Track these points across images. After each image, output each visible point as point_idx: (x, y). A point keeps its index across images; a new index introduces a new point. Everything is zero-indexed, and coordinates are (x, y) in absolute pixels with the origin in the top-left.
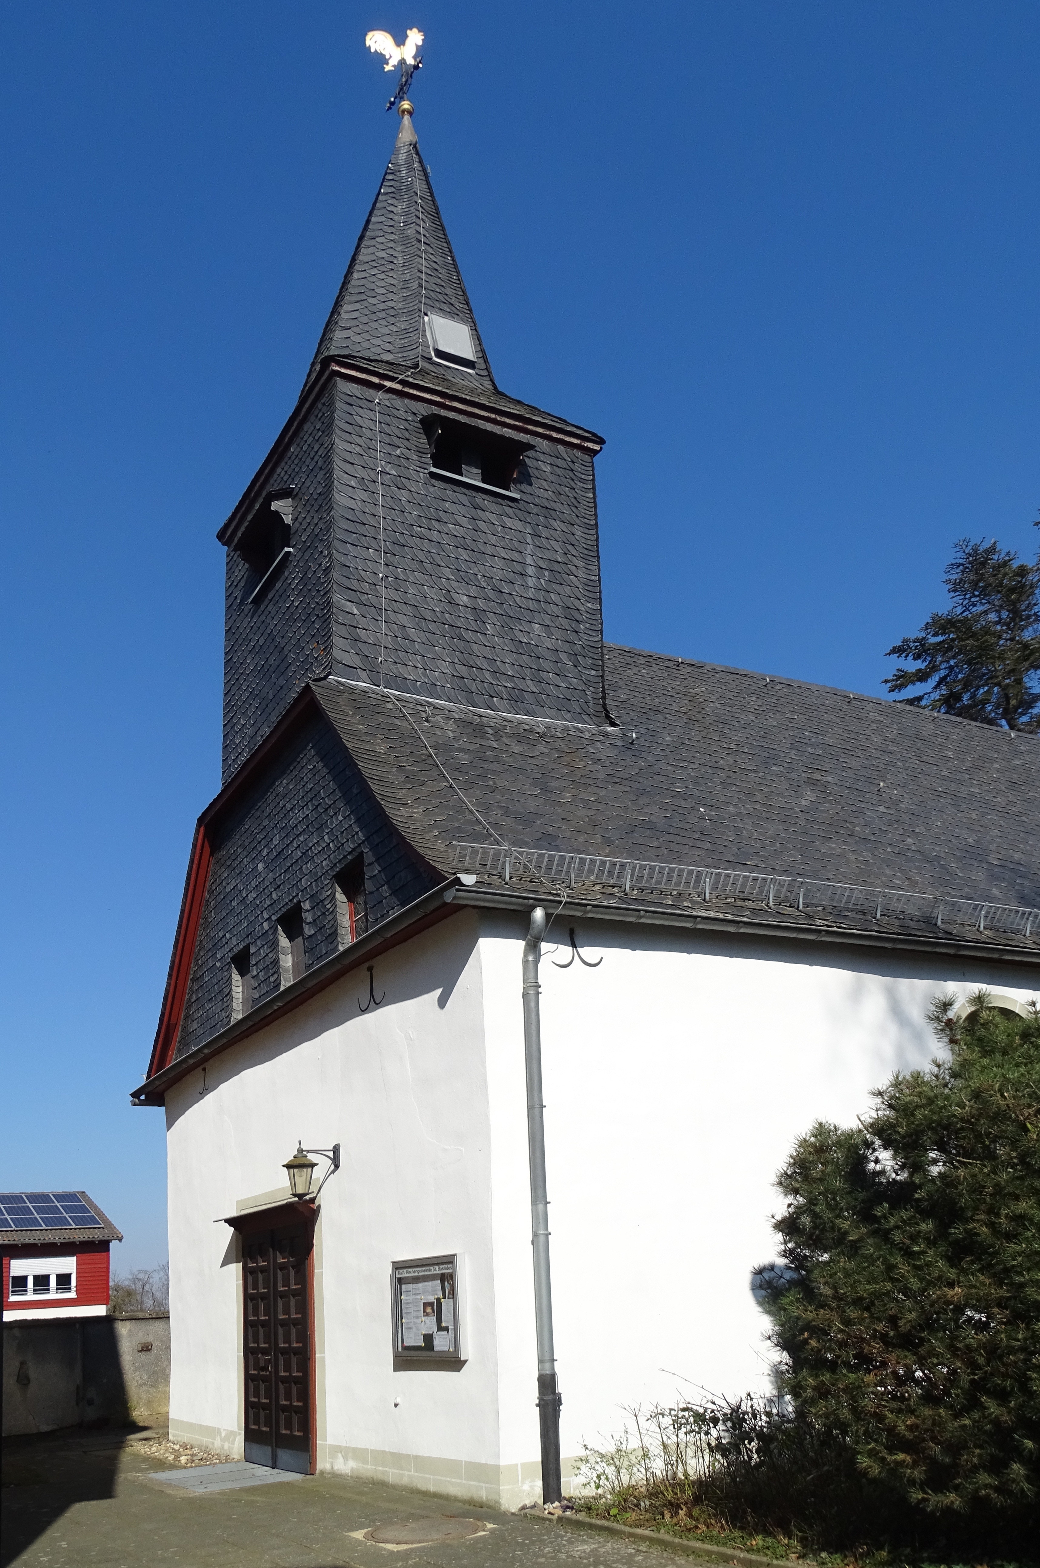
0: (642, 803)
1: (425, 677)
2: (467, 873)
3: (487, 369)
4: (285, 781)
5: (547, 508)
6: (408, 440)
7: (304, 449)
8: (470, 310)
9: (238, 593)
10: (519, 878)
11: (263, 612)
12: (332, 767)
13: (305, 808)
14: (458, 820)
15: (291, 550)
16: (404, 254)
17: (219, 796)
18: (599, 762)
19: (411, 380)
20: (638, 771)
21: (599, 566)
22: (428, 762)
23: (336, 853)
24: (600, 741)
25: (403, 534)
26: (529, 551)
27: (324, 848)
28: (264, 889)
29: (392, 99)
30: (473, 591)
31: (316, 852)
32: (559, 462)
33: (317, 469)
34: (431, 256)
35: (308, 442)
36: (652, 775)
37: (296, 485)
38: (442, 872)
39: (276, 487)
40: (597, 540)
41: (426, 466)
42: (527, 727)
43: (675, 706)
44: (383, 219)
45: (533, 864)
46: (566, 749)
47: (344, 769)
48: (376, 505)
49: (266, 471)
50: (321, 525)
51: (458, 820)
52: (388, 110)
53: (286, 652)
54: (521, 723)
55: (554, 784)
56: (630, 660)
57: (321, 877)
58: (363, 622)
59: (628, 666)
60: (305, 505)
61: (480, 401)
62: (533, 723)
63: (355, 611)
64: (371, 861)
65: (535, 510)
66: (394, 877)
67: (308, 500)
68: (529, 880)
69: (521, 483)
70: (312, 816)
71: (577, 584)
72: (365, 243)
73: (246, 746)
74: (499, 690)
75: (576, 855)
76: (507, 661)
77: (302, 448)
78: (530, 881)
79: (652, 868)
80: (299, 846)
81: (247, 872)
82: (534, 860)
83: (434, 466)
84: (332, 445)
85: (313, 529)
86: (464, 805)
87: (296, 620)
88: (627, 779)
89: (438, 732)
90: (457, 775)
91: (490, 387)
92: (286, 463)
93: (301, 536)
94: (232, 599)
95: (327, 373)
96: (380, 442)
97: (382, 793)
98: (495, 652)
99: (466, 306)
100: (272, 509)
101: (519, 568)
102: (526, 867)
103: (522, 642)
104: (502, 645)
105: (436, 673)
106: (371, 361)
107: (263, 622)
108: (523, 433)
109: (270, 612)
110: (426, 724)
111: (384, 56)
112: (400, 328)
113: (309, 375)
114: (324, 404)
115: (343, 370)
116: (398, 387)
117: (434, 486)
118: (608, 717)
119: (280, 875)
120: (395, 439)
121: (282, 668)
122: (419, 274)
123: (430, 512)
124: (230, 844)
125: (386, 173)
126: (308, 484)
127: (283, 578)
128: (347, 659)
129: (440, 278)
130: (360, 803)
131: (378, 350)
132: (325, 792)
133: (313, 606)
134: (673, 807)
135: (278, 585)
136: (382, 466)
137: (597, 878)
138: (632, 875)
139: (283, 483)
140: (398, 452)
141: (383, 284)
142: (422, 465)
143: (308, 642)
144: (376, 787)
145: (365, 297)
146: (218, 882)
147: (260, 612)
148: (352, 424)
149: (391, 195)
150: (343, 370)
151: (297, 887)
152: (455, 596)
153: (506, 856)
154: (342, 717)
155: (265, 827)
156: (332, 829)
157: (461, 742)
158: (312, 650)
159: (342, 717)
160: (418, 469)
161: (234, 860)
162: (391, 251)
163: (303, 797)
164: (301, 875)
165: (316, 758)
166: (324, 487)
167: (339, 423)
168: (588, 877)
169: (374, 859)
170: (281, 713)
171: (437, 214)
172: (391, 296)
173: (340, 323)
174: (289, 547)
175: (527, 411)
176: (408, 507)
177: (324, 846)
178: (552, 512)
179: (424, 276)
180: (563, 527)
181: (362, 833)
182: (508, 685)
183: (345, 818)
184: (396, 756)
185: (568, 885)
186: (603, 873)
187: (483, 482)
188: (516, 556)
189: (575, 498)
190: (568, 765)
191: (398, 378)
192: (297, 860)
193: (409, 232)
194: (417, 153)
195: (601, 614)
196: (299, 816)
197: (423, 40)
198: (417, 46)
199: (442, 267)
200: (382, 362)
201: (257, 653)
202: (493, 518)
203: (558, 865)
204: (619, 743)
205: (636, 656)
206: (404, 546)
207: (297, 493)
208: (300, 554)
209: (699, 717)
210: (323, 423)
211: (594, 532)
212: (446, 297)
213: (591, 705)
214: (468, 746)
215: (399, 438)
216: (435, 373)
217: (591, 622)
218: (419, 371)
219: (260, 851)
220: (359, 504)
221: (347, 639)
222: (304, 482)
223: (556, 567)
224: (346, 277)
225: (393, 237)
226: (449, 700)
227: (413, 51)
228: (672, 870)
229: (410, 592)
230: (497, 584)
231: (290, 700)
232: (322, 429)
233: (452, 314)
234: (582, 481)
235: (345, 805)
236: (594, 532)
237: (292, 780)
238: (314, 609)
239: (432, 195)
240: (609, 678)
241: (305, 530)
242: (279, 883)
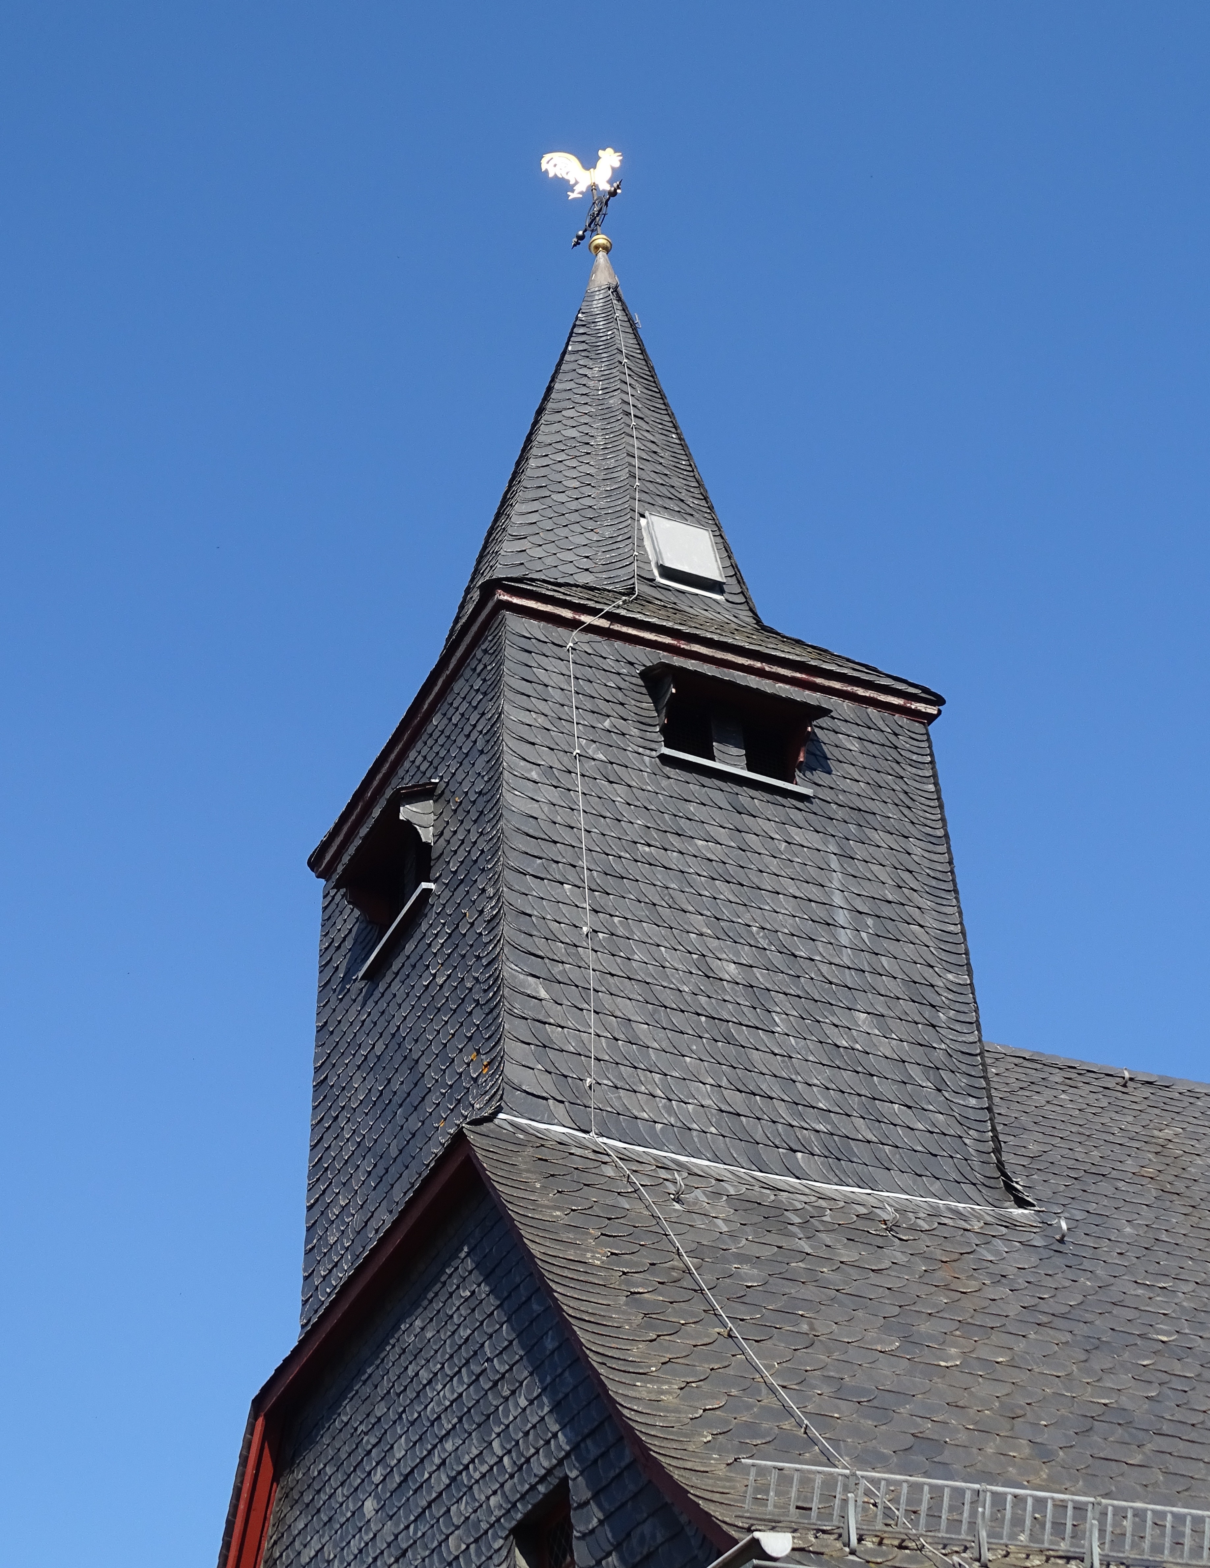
0: (1097, 1367)
1: (670, 1115)
2: (773, 1529)
3: (742, 593)
4: (418, 1323)
5: (860, 810)
6: (622, 704)
7: (454, 721)
8: (711, 508)
9: (341, 961)
10: (876, 1540)
11: (383, 994)
12: (505, 1294)
13: (455, 1379)
14: (749, 1407)
15: (432, 886)
16: (604, 432)
17: (296, 1352)
18: (1004, 1280)
19: (623, 612)
20: (1080, 1298)
21: (959, 907)
22: (685, 1284)
23: (516, 1479)
24: (1001, 1237)
25: (620, 857)
26: (836, 884)
27: (491, 1468)
28: (375, 1559)
29: (581, 233)
30: (746, 955)
31: (477, 1476)
32: (872, 735)
33: (475, 753)
34: (646, 434)
35: (461, 710)
36: (1109, 1307)
37: (441, 778)
38: (725, 1527)
39: (408, 782)
40: (950, 862)
41: (653, 746)
42: (862, 1210)
43: (1130, 1165)
44: (571, 385)
45: (903, 1507)
46: (939, 1255)
47: (529, 1299)
48: (573, 810)
49: (392, 757)
50: (481, 845)
51: (749, 1407)
52: (575, 245)
53: (422, 1068)
54: (850, 1202)
55: (925, 1327)
56: (1036, 1076)
57: (486, 1532)
58: (556, 1013)
59: (1034, 1087)
60: (455, 811)
61: (736, 643)
62: (872, 1201)
63: (543, 994)
64: (584, 1499)
65: (841, 813)
66: (629, 1535)
67: (461, 802)
68: (896, 1543)
69: (812, 769)
70: (468, 1396)
71: (926, 939)
72: (545, 417)
73: (347, 1249)
74: (804, 1137)
75: (985, 1486)
76: (816, 1082)
77: (450, 719)
78: (901, 1547)
79: (1139, 1514)
80: (444, 1462)
81: (343, 1520)
82: (903, 1499)
83: (666, 746)
84: (500, 714)
85: (469, 852)
86: (758, 1376)
87: (439, 1009)
88: (1063, 1316)
89: (699, 1222)
90: (742, 1311)
91: (751, 621)
92: (425, 743)
93: (448, 863)
94: (329, 971)
95: (490, 605)
96: (577, 708)
97: (601, 1350)
98: (793, 1065)
99: (703, 503)
100: (401, 818)
101: (820, 912)
102: (888, 1513)
103: (839, 1047)
104: (803, 1052)
105: (690, 1107)
106: (560, 585)
107: (383, 1013)
108: (809, 690)
109: (395, 995)
110: (677, 1206)
111: (568, 181)
112: (602, 535)
113: (462, 607)
114: (485, 651)
115: (516, 600)
116: (604, 623)
117: (669, 778)
118: (1010, 1188)
119: (407, 1527)
120: (601, 703)
121: (415, 1099)
122: (630, 459)
123: (664, 821)
124: (311, 1456)
125: (574, 326)
126: (460, 776)
127: (418, 935)
128: (529, 1081)
129: (661, 464)
130: (559, 1371)
131: (570, 569)
132: (493, 1347)
133: (469, 985)
134: (1159, 1374)
135: (409, 947)
136: (581, 747)
137: (1032, 1537)
138: (1102, 1531)
139: (419, 775)
140: (607, 724)
141: (574, 473)
142: (647, 744)
143: (461, 1050)
144: (589, 1336)
145: (548, 493)
146: (286, 1540)
147: (377, 995)
148: (531, 682)
149: (583, 354)
150: (516, 600)
151: (440, 1554)
152: (714, 964)
153: (846, 1490)
154: (521, 1194)
155: (379, 1419)
156: (507, 1426)
157: (744, 1241)
158: (468, 1064)
159: (521, 1194)
160: (641, 750)
161: (318, 1492)
162: (585, 429)
163: (451, 1356)
164: (447, 1528)
165: (476, 1277)
166: (487, 782)
167: (510, 680)
168: (1013, 1536)
169: (589, 1495)
170: (413, 1185)
171: (652, 376)
172: (587, 490)
173: (510, 530)
174: (429, 881)
175: (812, 656)
176: (627, 813)
177: (492, 1463)
178: (869, 817)
179: (636, 462)
180: (890, 840)
181: (565, 1436)
182: (820, 1127)
183: (531, 1402)
184: (624, 1273)
185: (977, 1555)
186: (1043, 1526)
187: (750, 769)
188: (814, 892)
189: (906, 793)
190: (947, 1288)
191: (602, 610)
192: (440, 1494)
193: (611, 402)
194: (619, 299)
195: (973, 993)
196: (444, 1396)
197: (621, 161)
198: (613, 169)
199: (663, 449)
200: (577, 586)
201: (372, 1069)
202: (770, 828)
203: (951, 1509)
204: (1038, 1242)
205: (1046, 1069)
206: (623, 878)
207: (443, 792)
208: (447, 894)
209: (1180, 1186)
210: (484, 680)
211: (943, 849)
212: (672, 490)
213: (976, 1165)
214: (756, 1250)
215: (608, 701)
216: (661, 600)
217: (957, 1006)
218: (636, 599)
219: (369, 1473)
220: (546, 809)
221: (529, 1044)
222: (454, 774)
223: (886, 910)
224: (518, 464)
225: (586, 409)
226: (716, 1159)
227: (608, 174)
228: (1179, 1519)
229: (636, 957)
230: (787, 941)
231: (429, 1160)
232: (483, 690)
233: (684, 515)
234: (914, 764)
235: (531, 1374)
236: (943, 849)
237: (431, 1320)
238: (471, 989)
239: (643, 352)
240: (1003, 1112)
241: (455, 852)
242: (404, 1546)
